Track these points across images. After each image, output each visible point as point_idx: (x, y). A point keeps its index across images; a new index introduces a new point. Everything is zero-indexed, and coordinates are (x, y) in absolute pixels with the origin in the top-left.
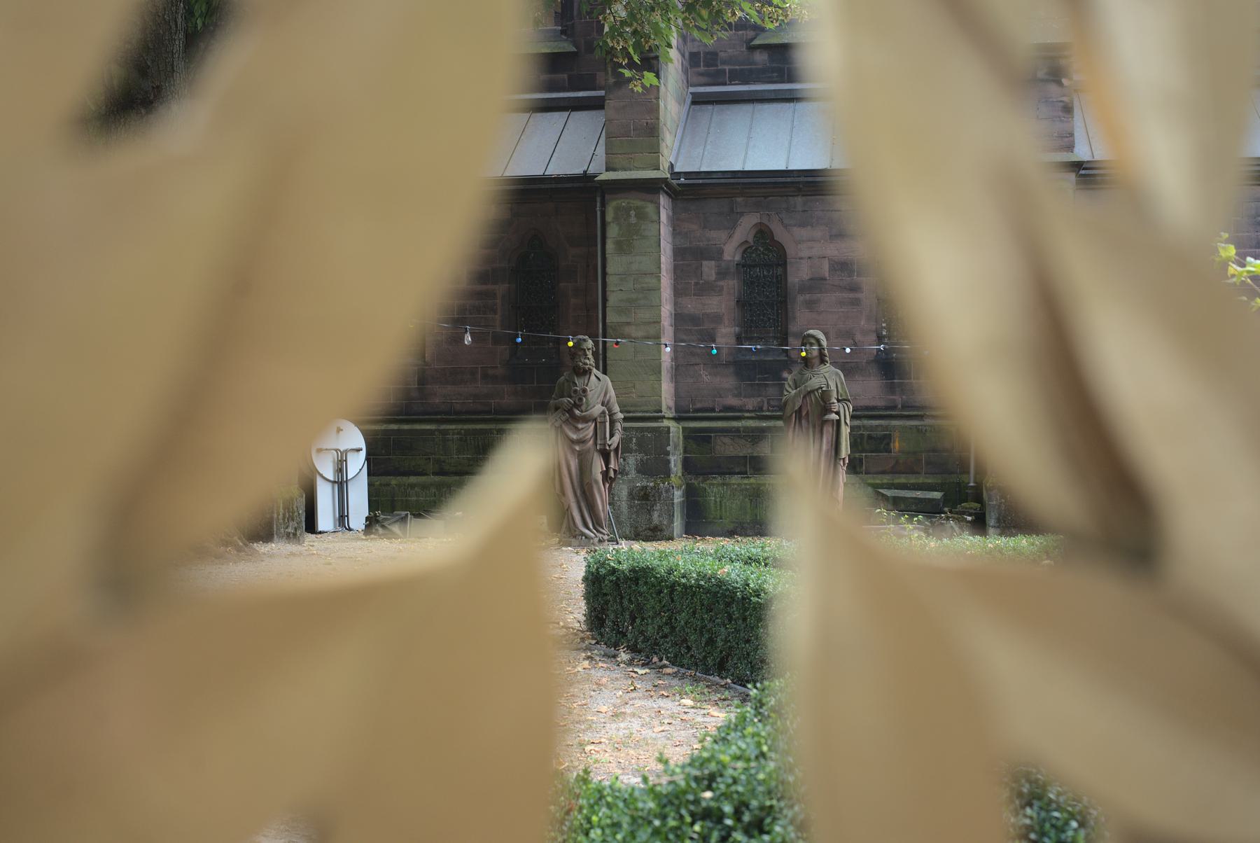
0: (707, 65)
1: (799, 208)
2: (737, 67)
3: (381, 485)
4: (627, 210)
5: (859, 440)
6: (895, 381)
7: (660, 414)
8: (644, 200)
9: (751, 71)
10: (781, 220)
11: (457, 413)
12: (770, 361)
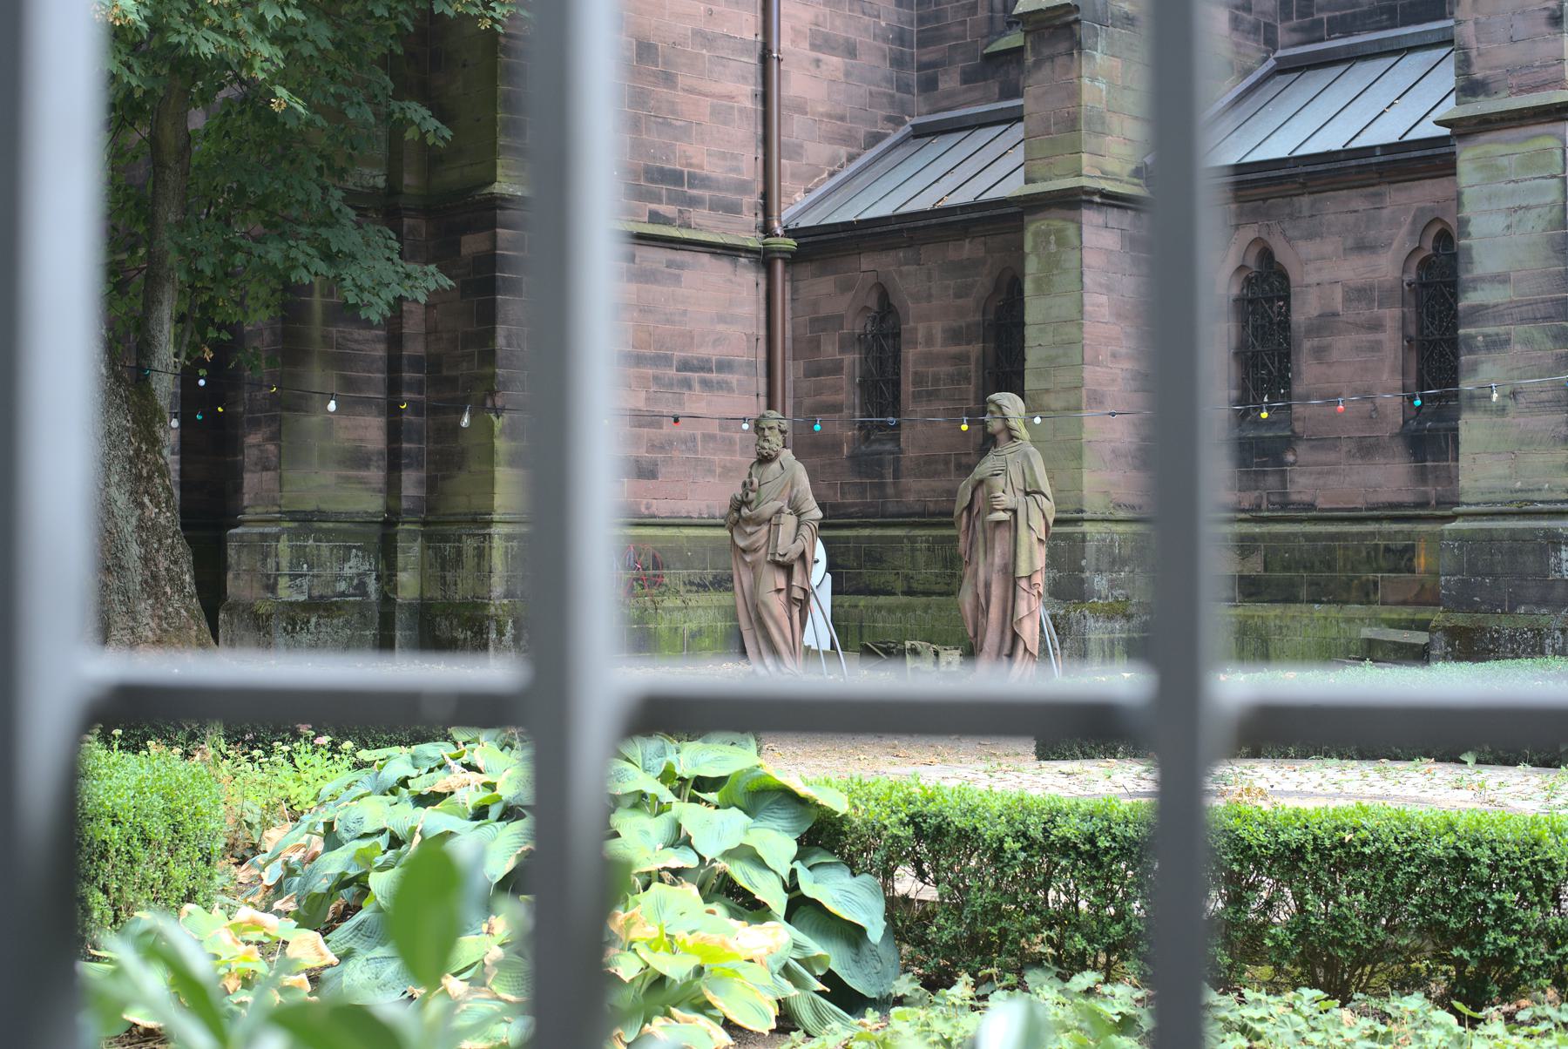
0: (1301, 15)
1: (1306, 213)
2: (1337, 13)
3: (850, 606)
4: (1047, 234)
5: (1373, 554)
6: (1427, 464)
7: (1080, 515)
8: (1064, 219)
9: (1354, 16)
10: (1283, 233)
11: (933, 515)
12: (1270, 437)
